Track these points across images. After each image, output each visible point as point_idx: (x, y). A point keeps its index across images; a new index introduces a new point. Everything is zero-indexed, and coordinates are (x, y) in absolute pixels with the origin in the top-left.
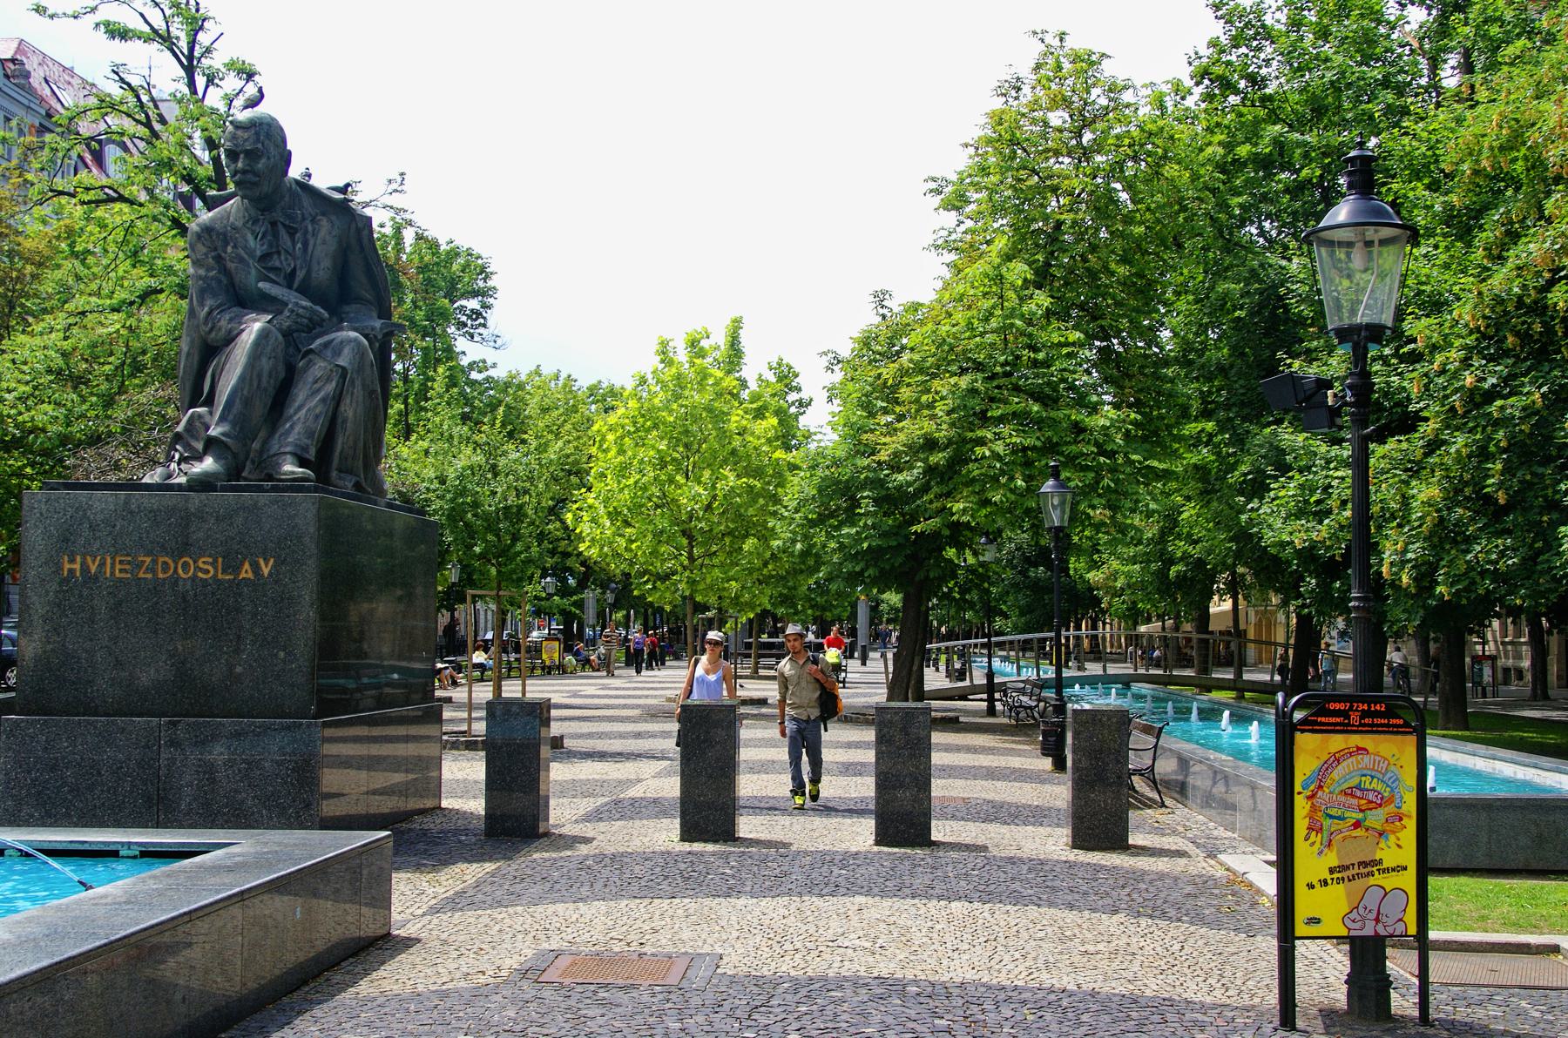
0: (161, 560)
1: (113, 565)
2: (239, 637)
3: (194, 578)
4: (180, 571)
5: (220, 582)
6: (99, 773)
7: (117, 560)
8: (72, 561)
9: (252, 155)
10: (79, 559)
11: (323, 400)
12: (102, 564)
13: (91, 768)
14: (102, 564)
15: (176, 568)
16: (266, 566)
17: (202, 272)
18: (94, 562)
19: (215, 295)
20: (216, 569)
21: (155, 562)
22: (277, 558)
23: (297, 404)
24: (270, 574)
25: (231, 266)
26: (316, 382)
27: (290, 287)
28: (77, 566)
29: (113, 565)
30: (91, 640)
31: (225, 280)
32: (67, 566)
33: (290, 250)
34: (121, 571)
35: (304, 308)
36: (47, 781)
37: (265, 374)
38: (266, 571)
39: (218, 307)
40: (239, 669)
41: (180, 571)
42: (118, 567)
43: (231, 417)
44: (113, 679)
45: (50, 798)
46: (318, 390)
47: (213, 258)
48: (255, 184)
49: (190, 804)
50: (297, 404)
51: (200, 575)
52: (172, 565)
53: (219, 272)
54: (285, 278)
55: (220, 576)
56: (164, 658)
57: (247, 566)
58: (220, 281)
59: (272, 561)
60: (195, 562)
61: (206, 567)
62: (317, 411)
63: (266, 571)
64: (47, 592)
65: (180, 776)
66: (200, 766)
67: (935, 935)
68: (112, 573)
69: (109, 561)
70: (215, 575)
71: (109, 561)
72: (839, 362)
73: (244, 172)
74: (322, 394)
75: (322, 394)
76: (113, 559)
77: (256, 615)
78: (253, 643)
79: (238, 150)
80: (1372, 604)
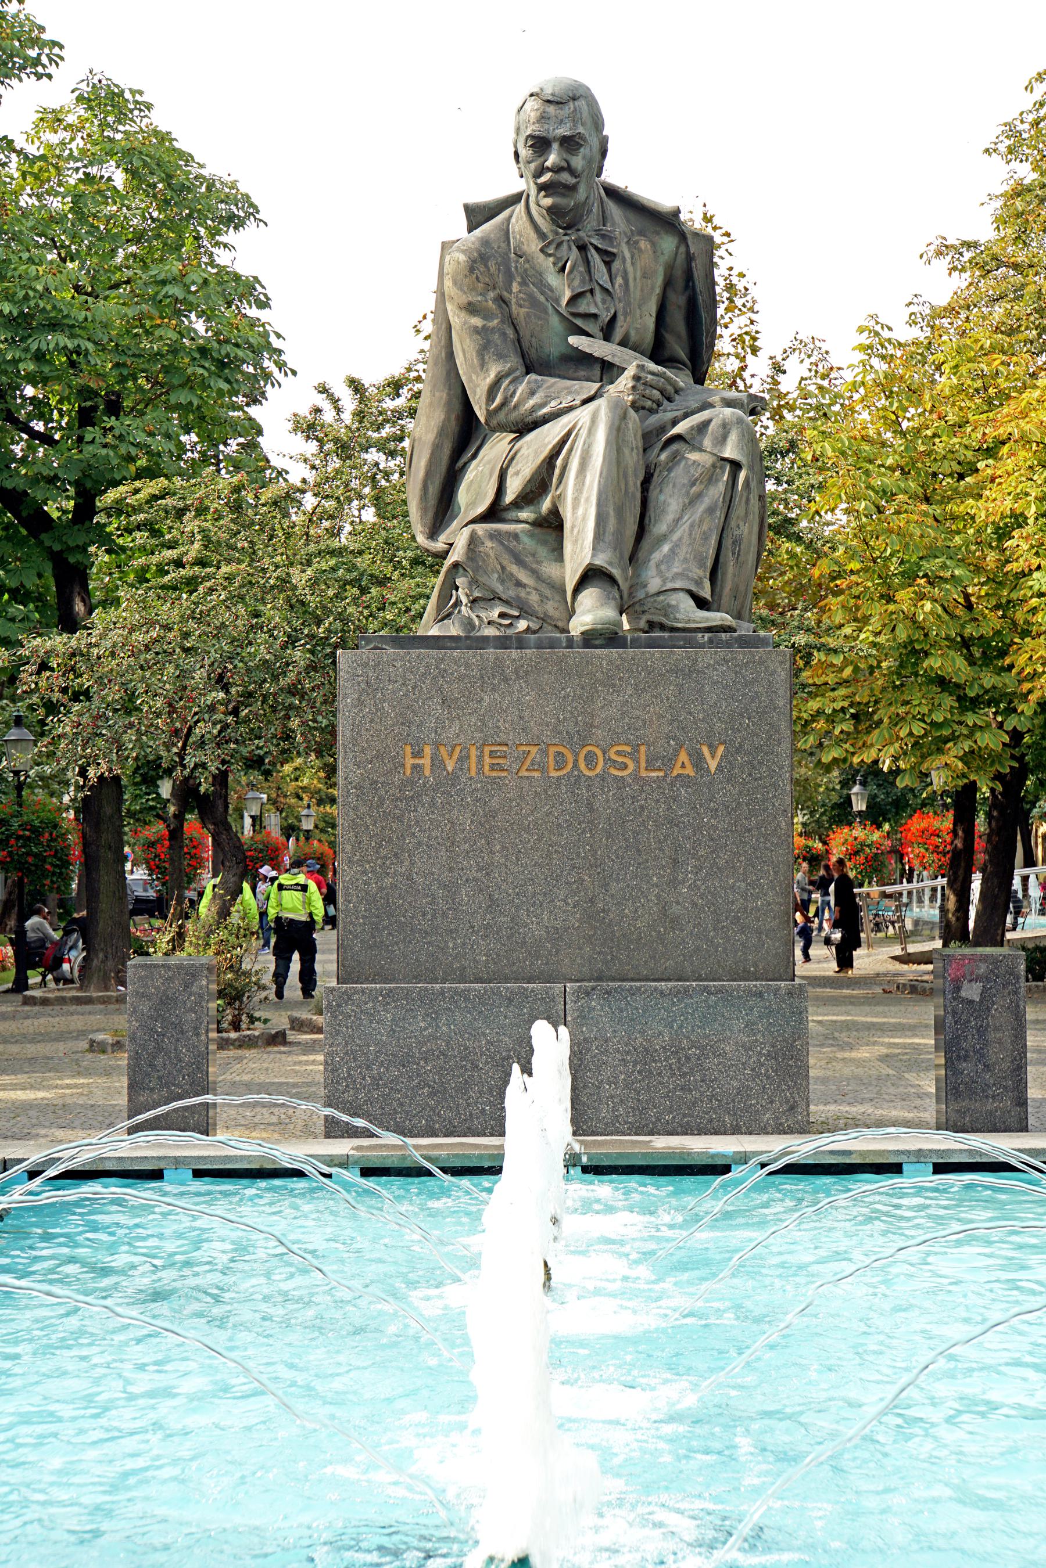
0: (553, 750)
1: (480, 758)
2: (675, 862)
4: (582, 765)
5: (646, 782)
6: (475, 1067)
7: (487, 749)
8: (418, 754)
9: (570, 143)
10: (428, 751)
11: (711, 510)
12: (464, 758)
13: (463, 1059)
14: (464, 758)
15: (576, 762)
16: (713, 757)
18: (451, 756)
21: (544, 753)
22: (727, 743)
24: (719, 768)
25: (520, 312)
26: (693, 484)
28: (426, 761)
29: (480, 758)
30: (451, 869)
31: (510, 333)
33: (608, 286)
34: (492, 767)
35: (653, 374)
36: (396, 1080)
37: (630, 471)
38: (713, 765)
40: (676, 909)
41: (582, 765)
42: (487, 760)
43: (608, 537)
44: (487, 927)
45: (401, 1104)
46: (699, 496)
47: (495, 300)
49: (614, 1109)
51: (614, 772)
52: (570, 759)
53: (502, 322)
54: (602, 330)
55: (644, 773)
56: (562, 894)
57: (683, 757)
58: (504, 334)
59: (721, 748)
60: (604, 753)
61: (620, 759)
62: (705, 527)
63: (713, 765)
64: (382, 801)
65: (598, 1067)
66: (628, 1053)
67: (425, 1338)
68: (480, 771)
69: (474, 752)
71: (474, 752)
77: (700, 828)
78: (698, 870)
79: (550, 136)
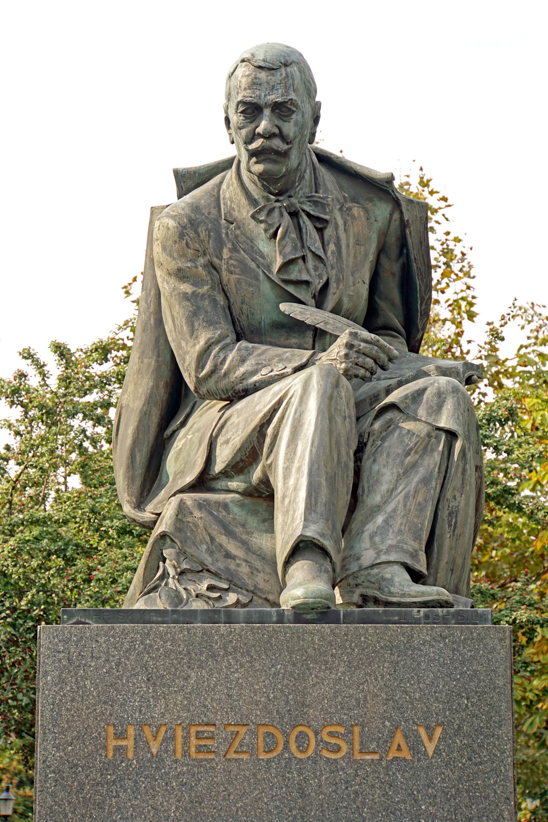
1: (186, 739)
3: (315, 759)
4: (293, 747)
5: (361, 764)
11: (426, 481)
15: (287, 743)
16: (430, 739)
17: (186, 288)
19: (210, 323)
20: (351, 743)
23: (384, 488)
26: (408, 454)
27: (319, 305)
28: (129, 743)
29: (186, 739)
32: (112, 743)
38: (430, 748)
39: (218, 342)
41: (293, 747)
42: (194, 741)
46: (414, 466)
47: (205, 266)
48: (285, 154)
50: (384, 488)
52: (281, 740)
53: (213, 288)
55: (358, 756)
60: (316, 734)
63: (430, 748)
68: (186, 753)
70: (351, 752)
71: (179, 733)
72: (198, 308)
73: (269, 136)
74: (422, 472)
75: (422, 472)
76: (187, 730)
79: (262, 102)
80: (398, 526)
